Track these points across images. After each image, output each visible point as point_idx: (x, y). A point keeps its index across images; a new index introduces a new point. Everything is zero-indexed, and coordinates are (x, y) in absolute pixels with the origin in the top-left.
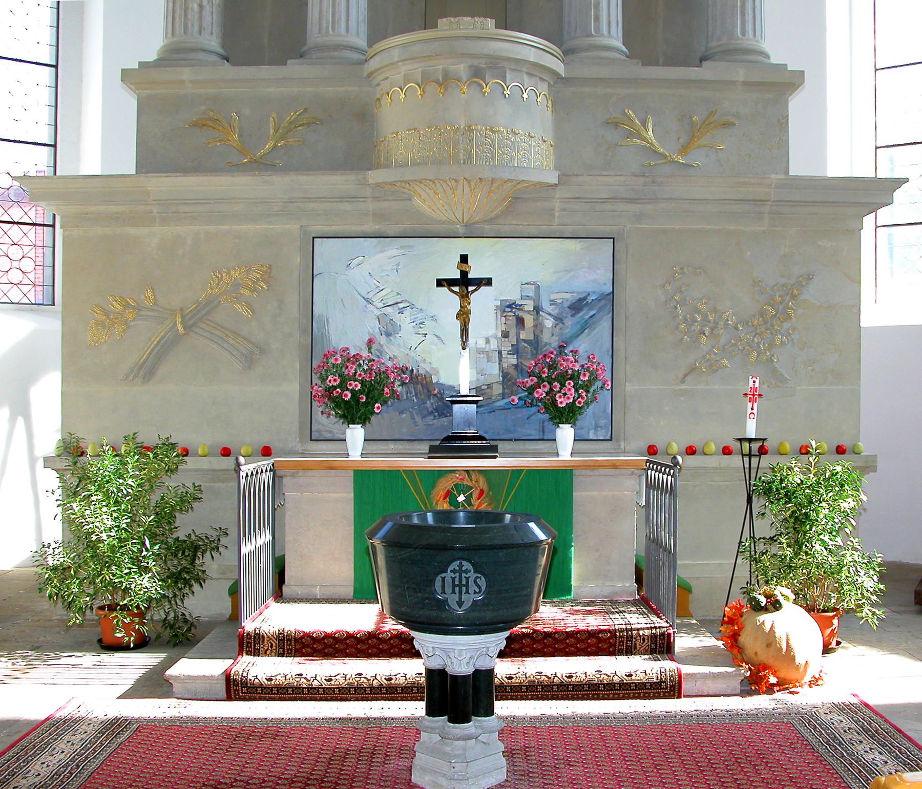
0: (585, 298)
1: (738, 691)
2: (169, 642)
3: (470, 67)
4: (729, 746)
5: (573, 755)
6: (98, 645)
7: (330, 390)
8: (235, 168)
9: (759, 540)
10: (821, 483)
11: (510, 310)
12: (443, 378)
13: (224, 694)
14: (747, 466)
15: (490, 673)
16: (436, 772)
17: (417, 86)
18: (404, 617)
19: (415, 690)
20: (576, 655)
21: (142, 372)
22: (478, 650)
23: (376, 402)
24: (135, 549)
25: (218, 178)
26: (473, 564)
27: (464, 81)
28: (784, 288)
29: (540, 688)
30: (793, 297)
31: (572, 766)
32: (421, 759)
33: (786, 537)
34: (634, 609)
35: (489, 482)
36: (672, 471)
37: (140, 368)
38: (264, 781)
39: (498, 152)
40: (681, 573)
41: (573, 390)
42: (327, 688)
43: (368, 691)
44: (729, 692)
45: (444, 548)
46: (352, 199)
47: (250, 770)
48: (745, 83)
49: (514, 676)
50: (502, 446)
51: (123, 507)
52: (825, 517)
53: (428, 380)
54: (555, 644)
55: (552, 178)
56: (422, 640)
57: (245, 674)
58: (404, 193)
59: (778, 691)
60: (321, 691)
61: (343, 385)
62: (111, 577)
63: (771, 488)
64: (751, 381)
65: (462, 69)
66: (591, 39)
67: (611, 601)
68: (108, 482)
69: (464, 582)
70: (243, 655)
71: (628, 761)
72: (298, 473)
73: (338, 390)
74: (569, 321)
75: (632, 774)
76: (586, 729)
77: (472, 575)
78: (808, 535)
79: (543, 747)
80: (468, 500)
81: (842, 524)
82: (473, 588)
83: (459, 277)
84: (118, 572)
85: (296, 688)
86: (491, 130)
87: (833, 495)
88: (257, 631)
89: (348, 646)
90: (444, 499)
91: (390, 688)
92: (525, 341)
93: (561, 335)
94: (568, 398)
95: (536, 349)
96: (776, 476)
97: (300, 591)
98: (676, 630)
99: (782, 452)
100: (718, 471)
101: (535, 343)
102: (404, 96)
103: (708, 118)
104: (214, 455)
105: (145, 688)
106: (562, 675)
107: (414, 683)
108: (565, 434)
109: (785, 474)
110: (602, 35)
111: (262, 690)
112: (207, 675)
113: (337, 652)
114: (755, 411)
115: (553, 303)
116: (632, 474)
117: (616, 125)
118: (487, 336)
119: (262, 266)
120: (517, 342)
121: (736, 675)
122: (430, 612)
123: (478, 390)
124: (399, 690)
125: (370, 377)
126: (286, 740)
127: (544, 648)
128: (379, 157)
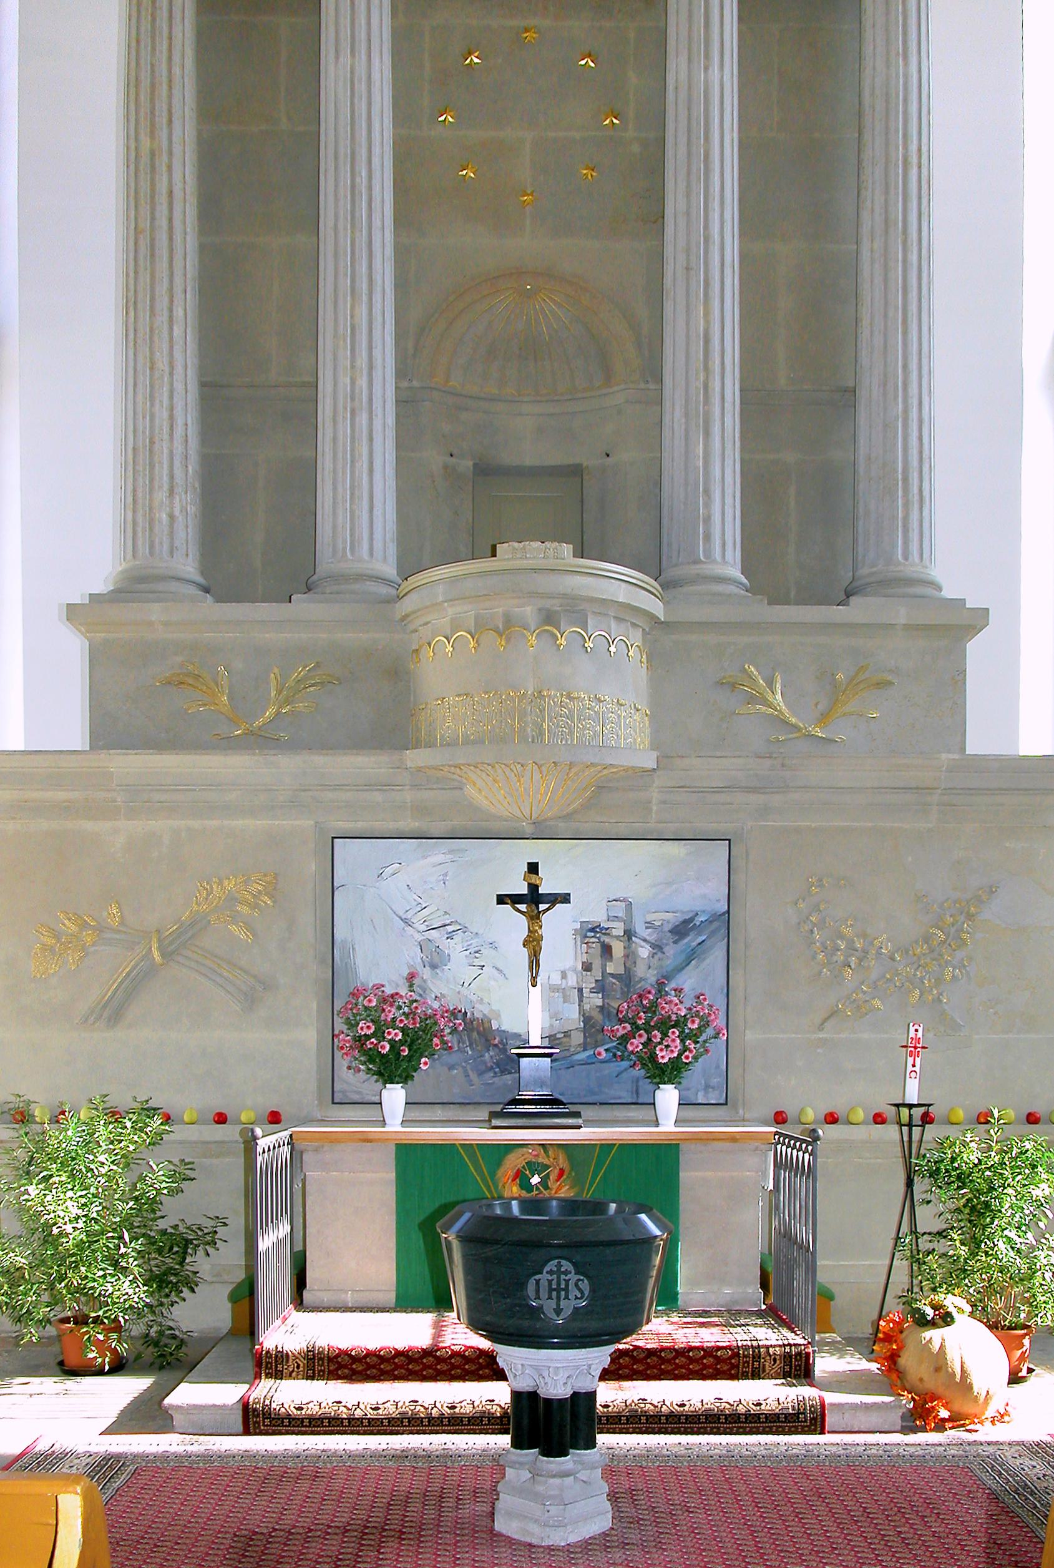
0: (691, 920)
1: (898, 1428)
2: (152, 1364)
3: (540, 610)
4: (889, 1493)
5: (692, 1500)
6: (57, 1368)
7: (360, 1040)
8: (227, 744)
9: (923, 1235)
10: (1005, 1164)
11: (593, 934)
12: (507, 1023)
13: (240, 1428)
14: (906, 1138)
15: (592, 1396)
16: (526, 1517)
17: (469, 636)
18: (488, 1327)
19: (485, 1421)
20: (689, 1379)
21: (106, 1014)
22: (577, 1367)
23: (422, 1056)
24: (111, 1245)
25: (207, 757)
26: (574, 1264)
27: (532, 630)
28: (957, 905)
29: (643, 1419)
30: (970, 917)
31: (692, 1512)
32: (505, 1501)
33: (959, 1232)
34: (759, 1321)
35: (570, 1158)
36: (810, 1148)
37: (104, 1007)
38: (311, 1530)
39: (578, 727)
40: (822, 1277)
41: (678, 1041)
42: (373, 1419)
43: (426, 1422)
44: (886, 1428)
45: (538, 1245)
46: (384, 786)
47: (289, 1519)
48: (907, 627)
49: (611, 1404)
50: (587, 1112)
51: (93, 1190)
52: (1011, 1207)
53: (486, 1025)
54: (661, 1365)
55: (649, 761)
56: (508, 1356)
57: (267, 1402)
58: (453, 780)
59: (950, 1428)
60: (365, 1422)
61: (379, 1034)
62: (80, 1282)
63: (938, 1169)
64: (912, 1029)
65: (529, 612)
66: (698, 566)
67: (729, 1311)
68: (73, 1159)
69: (563, 1286)
70: (261, 1379)
71: (761, 1508)
72: (323, 1147)
73: (373, 1040)
74: (671, 950)
75: (768, 1523)
76: (707, 1470)
77: (573, 1277)
78: (989, 1230)
79: (654, 1490)
80: (544, 1182)
81: (1034, 1216)
82: (574, 1292)
83: (526, 892)
84: (89, 1274)
85: (333, 1419)
86: (569, 697)
87: (1023, 1179)
88: (280, 1349)
89: (397, 1367)
90: (513, 1180)
91: (453, 1418)
92: (612, 975)
93: (661, 967)
94: (672, 1051)
95: (628, 986)
96: (945, 1154)
97: (326, 1298)
98: (816, 1348)
99: (954, 1120)
100: (868, 1145)
101: (626, 978)
102: (451, 649)
103: (857, 674)
104: (205, 1123)
105: (134, 1422)
106: (672, 1403)
107: (485, 1412)
108: (668, 1097)
109: (957, 1150)
110: (714, 561)
111: (289, 1422)
112: (218, 1404)
113: (382, 1375)
114: (917, 1069)
115: (649, 925)
116: (756, 1149)
117: (733, 686)
118: (562, 969)
119: (265, 875)
120: (602, 976)
121: (895, 1407)
122: (521, 1322)
123: (552, 1040)
124: (465, 1421)
125: (414, 1023)
126: (329, 1482)
127: (646, 1370)
128: (418, 730)
